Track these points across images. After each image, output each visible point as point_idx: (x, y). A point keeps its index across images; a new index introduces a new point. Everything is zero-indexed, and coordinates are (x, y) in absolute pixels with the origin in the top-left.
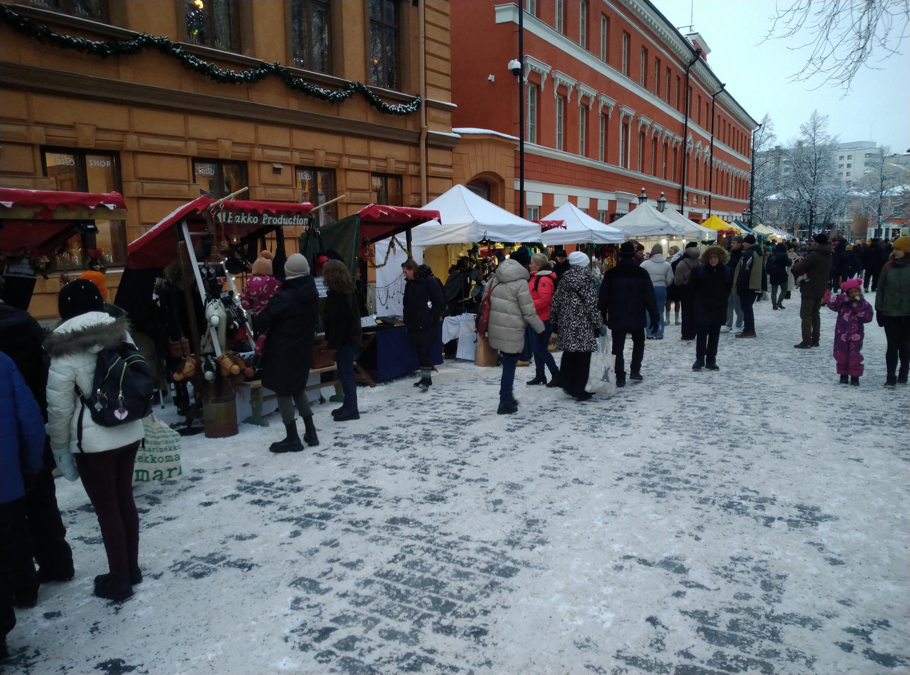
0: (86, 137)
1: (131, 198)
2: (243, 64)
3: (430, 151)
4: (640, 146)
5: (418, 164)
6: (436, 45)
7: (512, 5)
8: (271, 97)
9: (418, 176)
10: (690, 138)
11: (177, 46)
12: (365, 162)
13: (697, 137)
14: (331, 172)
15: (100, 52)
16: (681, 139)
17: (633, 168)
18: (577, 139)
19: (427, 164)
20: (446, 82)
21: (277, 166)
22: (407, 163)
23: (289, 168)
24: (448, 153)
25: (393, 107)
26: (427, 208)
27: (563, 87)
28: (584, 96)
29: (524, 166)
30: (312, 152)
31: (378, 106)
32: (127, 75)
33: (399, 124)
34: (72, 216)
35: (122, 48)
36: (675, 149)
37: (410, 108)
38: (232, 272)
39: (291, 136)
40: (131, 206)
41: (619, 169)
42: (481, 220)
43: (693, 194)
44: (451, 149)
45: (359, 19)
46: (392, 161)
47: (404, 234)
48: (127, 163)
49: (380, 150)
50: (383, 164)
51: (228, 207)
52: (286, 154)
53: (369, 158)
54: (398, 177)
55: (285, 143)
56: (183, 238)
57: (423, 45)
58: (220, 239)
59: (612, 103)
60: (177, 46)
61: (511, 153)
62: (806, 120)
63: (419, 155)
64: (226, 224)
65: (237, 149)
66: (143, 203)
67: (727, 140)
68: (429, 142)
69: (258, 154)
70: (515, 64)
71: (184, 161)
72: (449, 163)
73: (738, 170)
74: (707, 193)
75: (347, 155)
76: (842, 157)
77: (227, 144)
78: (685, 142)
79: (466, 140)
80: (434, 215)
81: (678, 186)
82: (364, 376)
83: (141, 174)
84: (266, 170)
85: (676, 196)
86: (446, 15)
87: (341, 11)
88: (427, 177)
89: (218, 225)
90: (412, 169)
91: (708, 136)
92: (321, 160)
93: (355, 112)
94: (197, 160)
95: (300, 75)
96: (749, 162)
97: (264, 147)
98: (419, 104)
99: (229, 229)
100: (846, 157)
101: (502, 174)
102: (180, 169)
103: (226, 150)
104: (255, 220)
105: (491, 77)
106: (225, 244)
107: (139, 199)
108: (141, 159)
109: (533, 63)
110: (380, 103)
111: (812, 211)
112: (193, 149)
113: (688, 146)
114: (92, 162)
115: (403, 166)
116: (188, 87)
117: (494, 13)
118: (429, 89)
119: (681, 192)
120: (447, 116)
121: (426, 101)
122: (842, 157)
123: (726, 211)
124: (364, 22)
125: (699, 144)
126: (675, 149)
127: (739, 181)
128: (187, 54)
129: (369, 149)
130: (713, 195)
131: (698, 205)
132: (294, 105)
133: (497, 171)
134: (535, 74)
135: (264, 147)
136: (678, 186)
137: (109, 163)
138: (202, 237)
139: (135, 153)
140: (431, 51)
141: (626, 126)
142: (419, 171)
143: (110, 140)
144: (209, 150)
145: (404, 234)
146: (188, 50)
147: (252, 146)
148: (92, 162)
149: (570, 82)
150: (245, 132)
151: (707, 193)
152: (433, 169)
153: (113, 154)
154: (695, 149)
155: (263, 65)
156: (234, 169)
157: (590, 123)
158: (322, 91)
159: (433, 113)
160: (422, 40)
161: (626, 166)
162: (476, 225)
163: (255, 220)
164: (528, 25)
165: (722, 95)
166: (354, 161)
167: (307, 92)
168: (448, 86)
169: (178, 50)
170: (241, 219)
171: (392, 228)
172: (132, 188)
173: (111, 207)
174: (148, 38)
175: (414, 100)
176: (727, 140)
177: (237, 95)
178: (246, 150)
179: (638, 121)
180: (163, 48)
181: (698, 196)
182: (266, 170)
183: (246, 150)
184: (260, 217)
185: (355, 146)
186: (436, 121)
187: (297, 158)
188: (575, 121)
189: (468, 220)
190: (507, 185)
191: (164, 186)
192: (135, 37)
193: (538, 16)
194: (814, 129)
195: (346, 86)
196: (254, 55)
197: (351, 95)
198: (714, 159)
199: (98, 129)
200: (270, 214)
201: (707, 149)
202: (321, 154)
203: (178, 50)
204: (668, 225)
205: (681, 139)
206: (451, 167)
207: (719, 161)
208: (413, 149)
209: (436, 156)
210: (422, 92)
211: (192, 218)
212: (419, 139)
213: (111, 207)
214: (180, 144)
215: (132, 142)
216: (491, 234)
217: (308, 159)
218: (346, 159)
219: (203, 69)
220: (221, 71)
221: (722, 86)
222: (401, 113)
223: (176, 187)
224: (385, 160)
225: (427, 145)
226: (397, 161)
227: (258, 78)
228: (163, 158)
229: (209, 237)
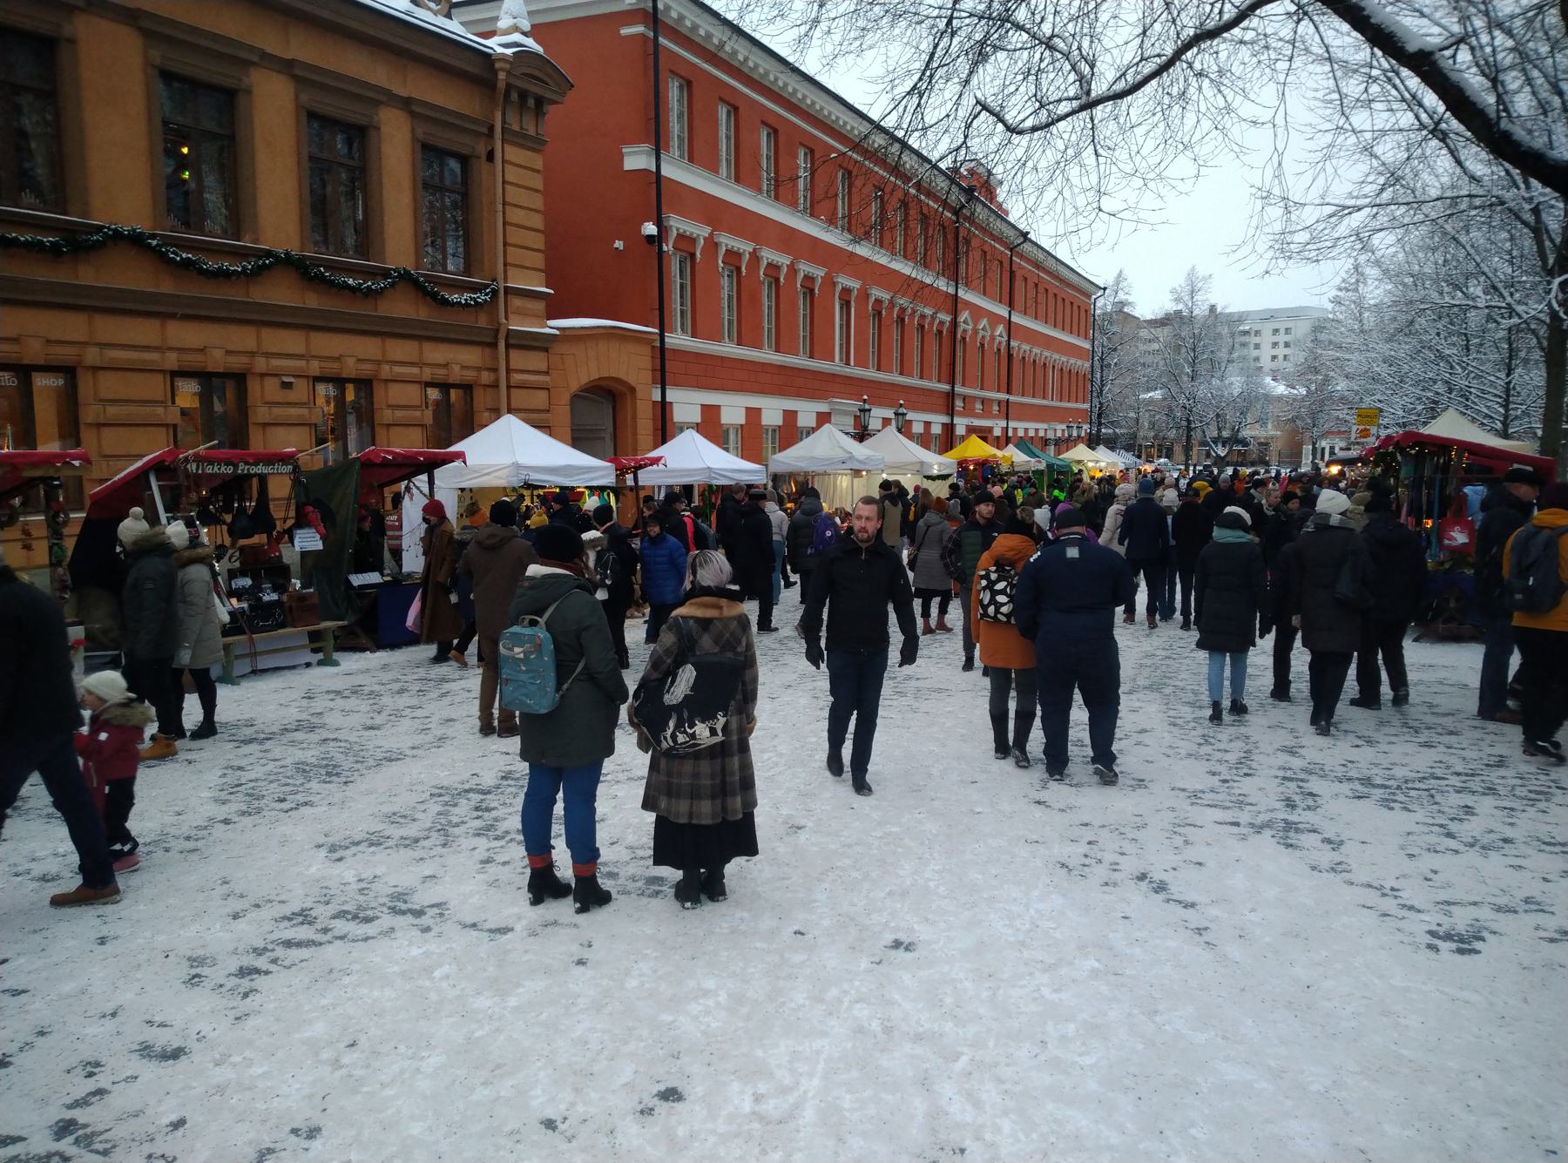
0: (34, 352)
1: (90, 425)
2: (243, 254)
3: (513, 353)
4: (871, 331)
5: (495, 370)
6: (523, 212)
7: (645, 147)
8: (281, 293)
9: (495, 386)
10: (964, 316)
11: (153, 236)
12: (415, 370)
13: (977, 312)
14: (365, 385)
15: (55, 250)
16: (947, 318)
17: (862, 363)
18: (760, 327)
19: (508, 371)
20: (538, 260)
21: (286, 379)
22: (479, 369)
23: (304, 381)
24: (542, 354)
25: (455, 297)
26: (453, 449)
27: (733, 256)
28: (769, 265)
29: (665, 367)
30: (338, 359)
31: (434, 296)
32: (88, 275)
33: (466, 319)
34: (38, 473)
35: (80, 243)
36: (940, 332)
37: (481, 298)
38: (204, 524)
39: (307, 340)
40: (87, 436)
41: (835, 366)
42: (524, 460)
43: (975, 398)
44: (546, 350)
45: (406, 184)
46: (456, 368)
47: (424, 477)
48: (85, 384)
49: (437, 353)
50: (443, 372)
51: (198, 458)
52: (302, 363)
53: (420, 364)
54: (467, 388)
55: (300, 349)
56: (150, 488)
57: (500, 215)
58: (188, 489)
59: (819, 272)
60: (153, 236)
61: (646, 351)
62: (1180, 281)
63: (496, 358)
64: (196, 475)
65: (231, 359)
66: (106, 431)
67: (1051, 315)
68: (512, 341)
69: (261, 364)
70: (650, 229)
71: (160, 377)
72: (544, 367)
73: (1064, 359)
74: (1003, 396)
75: (388, 362)
76: (1276, 331)
77: (218, 354)
78: (954, 323)
79: (568, 336)
80: (460, 456)
81: (946, 387)
82: (364, 641)
83: (104, 394)
84: (271, 385)
85: (942, 401)
86: (538, 171)
87: (380, 175)
88: (509, 387)
89: (188, 475)
90: (486, 377)
91: (1002, 311)
92: (350, 368)
93: (402, 307)
94: (175, 374)
95: (319, 263)
96: (1087, 345)
97: (268, 355)
98: (495, 293)
99: (198, 481)
100: (1282, 331)
101: (631, 380)
102: (155, 387)
103: (217, 361)
104: (230, 470)
105: (619, 244)
106: (194, 496)
107: (99, 425)
108: (107, 433)
109: (678, 224)
110: (437, 293)
111: (1189, 421)
112: (172, 361)
113: (962, 326)
114: (42, 382)
115: (474, 373)
116: (167, 286)
117: (622, 156)
118: (511, 272)
119: (951, 396)
120: (540, 306)
121: (506, 288)
122: (1276, 331)
123: (1042, 421)
124: (414, 188)
125: (984, 322)
126: (940, 332)
127: (1067, 375)
128: (164, 245)
129: (421, 352)
130: (1012, 398)
131: (986, 414)
132: (312, 300)
133: (622, 376)
134: (685, 240)
135: (268, 355)
136: (946, 387)
137: (61, 382)
138: (171, 488)
139: (96, 369)
140: (514, 220)
141: (846, 305)
142: (497, 379)
143: (64, 354)
144: (193, 361)
145: (424, 477)
146: (167, 241)
147: (253, 354)
148: (42, 382)
149: (745, 247)
150: (243, 338)
151: (1003, 396)
152: (517, 377)
153: (69, 371)
154: (975, 331)
155: (268, 254)
156: (226, 387)
157: (782, 304)
158: (351, 281)
159: (517, 302)
160: (500, 207)
161: (848, 363)
162: (517, 466)
163: (230, 470)
164: (667, 171)
165: (1027, 247)
166: (398, 369)
167: (330, 284)
168: (541, 265)
169: (154, 243)
170: (209, 470)
171: (408, 471)
172: (89, 413)
173: (77, 463)
174: (115, 231)
175: (487, 286)
176: (1051, 315)
177: (233, 293)
178: (244, 360)
179: (868, 296)
180: (136, 240)
181: (983, 400)
182: (271, 385)
183: (244, 360)
184: (236, 466)
185: (401, 350)
186: (523, 313)
187: (315, 368)
188: (755, 300)
189: (506, 460)
190: (640, 394)
191: (133, 409)
192: (99, 229)
193: (691, 160)
194: (1192, 293)
195: (386, 273)
196: (256, 241)
197: (393, 285)
198: (1013, 343)
199: (49, 341)
200: (247, 463)
201: (1000, 329)
202: (351, 362)
203: (154, 243)
204: (852, 457)
205: (947, 318)
206: (547, 373)
207: (1025, 347)
208: (488, 351)
209: (519, 359)
210: (500, 276)
211: (160, 468)
212: (496, 337)
213: (77, 463)
214: (155, 356)
215: (92, 356)
216: (535, 477)
217: (332, 368)
218: (386, 367)
219: (187, 263)
220: (211, 264)
221: (1025, 235)
222: (467, 305)
223: (148, 409)
224: (446, 366)
225: (508, 346)
226: (463, 367)
227: (259, 271)
228: (128, 374)
229: (178, 487)
